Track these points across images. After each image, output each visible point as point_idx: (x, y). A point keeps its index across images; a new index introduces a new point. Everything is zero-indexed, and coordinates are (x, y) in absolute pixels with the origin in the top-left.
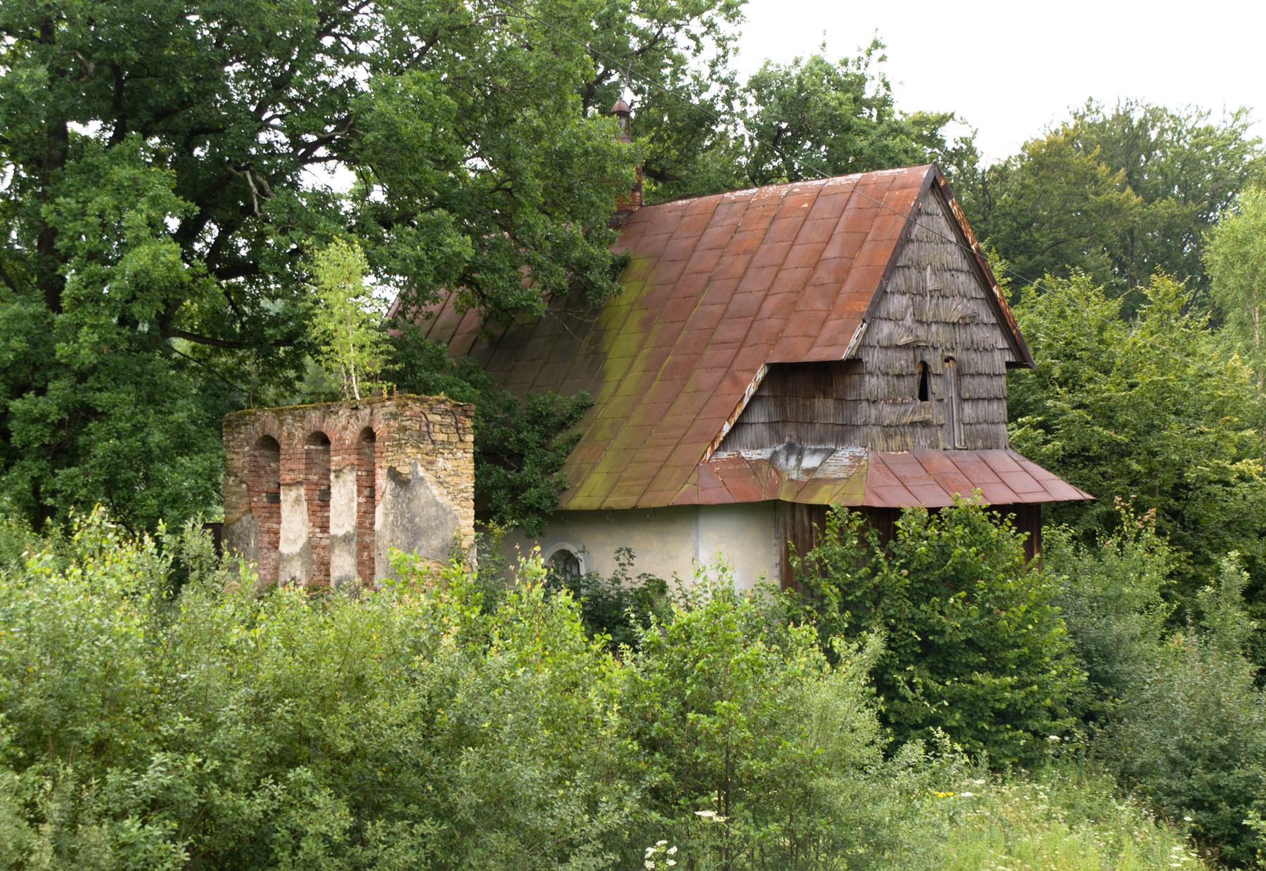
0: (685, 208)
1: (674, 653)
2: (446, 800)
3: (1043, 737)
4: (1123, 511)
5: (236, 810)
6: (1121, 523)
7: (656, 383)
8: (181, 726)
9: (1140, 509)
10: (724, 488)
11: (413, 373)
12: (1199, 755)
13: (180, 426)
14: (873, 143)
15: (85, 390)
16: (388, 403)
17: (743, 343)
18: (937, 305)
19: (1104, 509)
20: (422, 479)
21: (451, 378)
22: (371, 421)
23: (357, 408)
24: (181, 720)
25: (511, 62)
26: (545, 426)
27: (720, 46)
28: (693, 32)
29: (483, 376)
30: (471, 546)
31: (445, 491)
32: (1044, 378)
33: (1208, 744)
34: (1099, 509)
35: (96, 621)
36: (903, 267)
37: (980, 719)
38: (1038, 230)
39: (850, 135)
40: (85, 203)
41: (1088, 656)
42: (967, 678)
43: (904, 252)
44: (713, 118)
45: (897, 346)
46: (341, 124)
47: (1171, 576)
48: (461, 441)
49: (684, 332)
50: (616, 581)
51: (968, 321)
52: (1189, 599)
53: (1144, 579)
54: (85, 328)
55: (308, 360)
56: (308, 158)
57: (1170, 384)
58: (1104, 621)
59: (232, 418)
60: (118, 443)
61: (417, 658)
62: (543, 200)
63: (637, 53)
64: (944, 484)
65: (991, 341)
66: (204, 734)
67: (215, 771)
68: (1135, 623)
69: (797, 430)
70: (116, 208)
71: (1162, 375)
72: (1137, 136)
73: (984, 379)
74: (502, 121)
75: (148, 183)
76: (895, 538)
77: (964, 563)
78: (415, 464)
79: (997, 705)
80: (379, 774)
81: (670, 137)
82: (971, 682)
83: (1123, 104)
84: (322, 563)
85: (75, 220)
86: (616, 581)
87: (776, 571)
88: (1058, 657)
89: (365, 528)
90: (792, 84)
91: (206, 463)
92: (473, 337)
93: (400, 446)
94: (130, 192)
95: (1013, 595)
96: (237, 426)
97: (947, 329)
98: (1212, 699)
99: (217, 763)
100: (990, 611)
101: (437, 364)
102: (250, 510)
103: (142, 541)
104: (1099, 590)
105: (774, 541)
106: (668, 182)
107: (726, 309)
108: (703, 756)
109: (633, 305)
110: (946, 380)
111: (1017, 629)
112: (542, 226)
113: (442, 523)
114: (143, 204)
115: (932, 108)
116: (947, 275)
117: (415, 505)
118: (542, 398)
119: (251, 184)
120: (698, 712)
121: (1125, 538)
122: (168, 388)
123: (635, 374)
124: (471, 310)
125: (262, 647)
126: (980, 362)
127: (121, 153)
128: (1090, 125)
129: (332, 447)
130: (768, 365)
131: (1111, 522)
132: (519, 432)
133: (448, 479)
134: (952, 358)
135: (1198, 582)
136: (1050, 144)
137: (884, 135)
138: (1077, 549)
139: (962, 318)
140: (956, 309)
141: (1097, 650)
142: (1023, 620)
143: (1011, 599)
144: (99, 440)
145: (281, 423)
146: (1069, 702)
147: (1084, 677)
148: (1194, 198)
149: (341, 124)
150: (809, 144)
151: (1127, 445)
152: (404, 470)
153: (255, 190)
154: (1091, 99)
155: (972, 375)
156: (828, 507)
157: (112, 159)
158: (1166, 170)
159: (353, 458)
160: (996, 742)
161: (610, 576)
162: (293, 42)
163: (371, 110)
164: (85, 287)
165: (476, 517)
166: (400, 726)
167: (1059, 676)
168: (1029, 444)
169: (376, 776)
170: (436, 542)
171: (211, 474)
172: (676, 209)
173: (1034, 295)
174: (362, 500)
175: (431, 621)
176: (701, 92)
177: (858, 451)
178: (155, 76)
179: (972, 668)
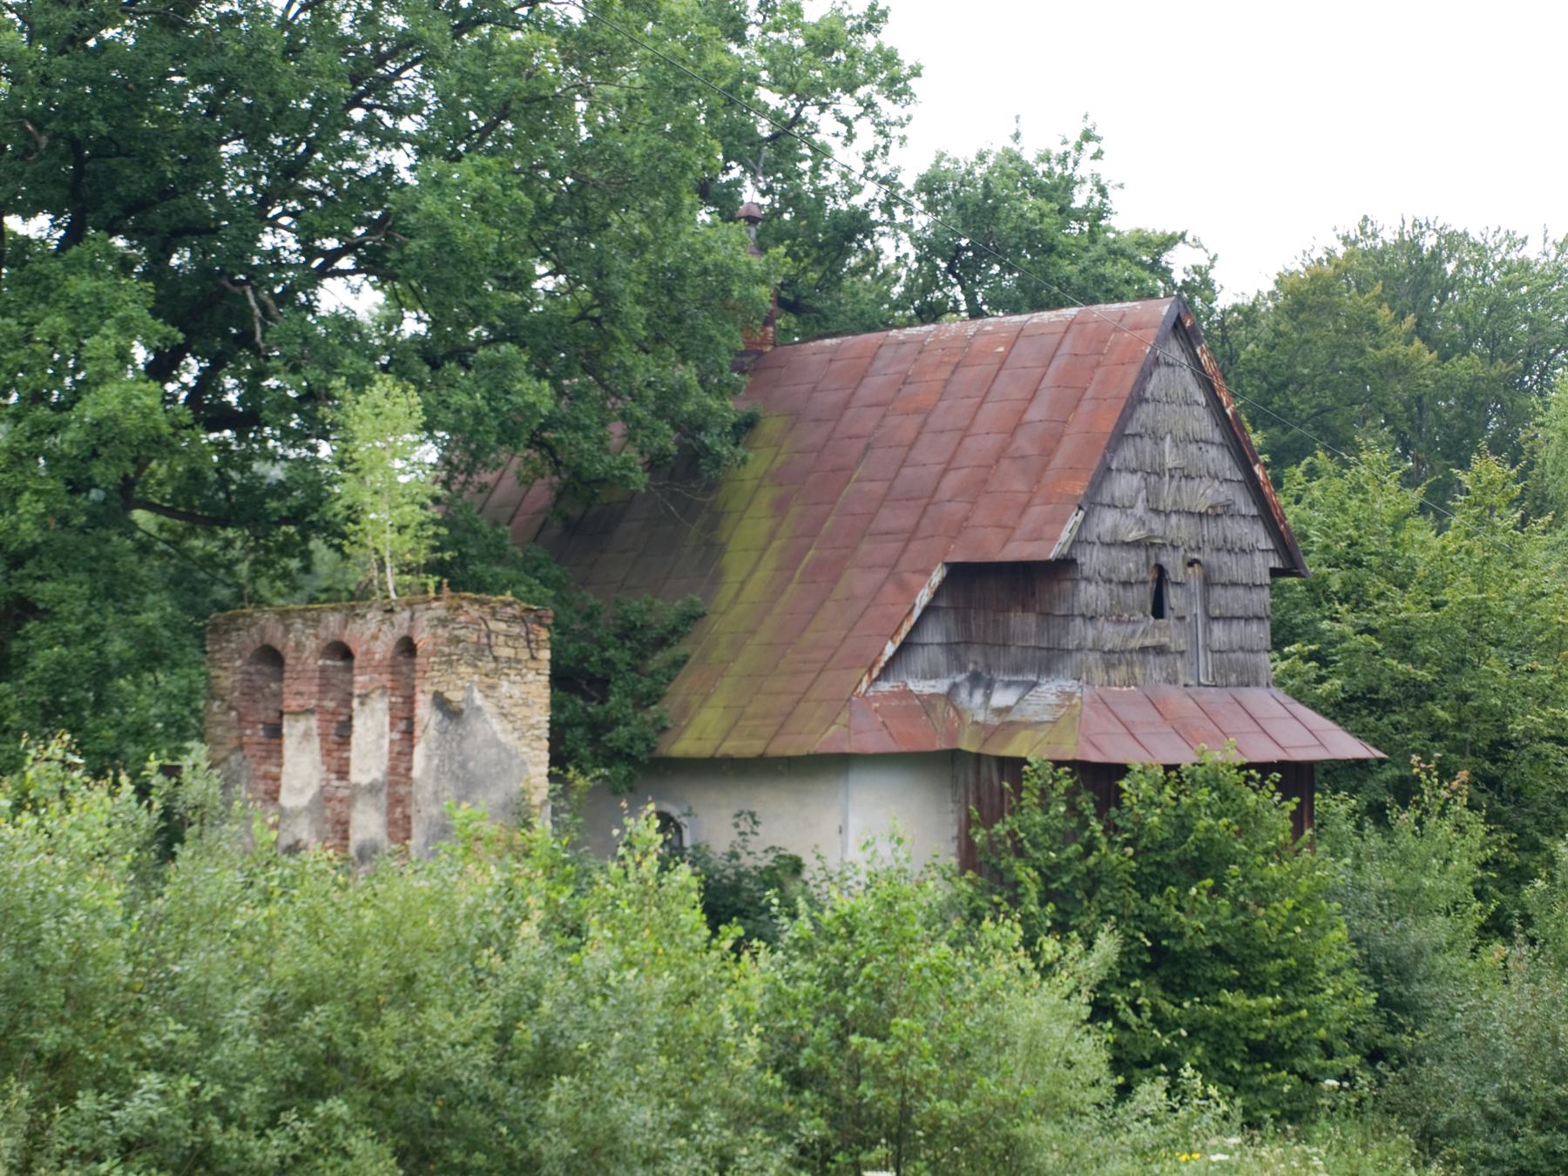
0: (835, 349)
1: (829, 953)
2: (524, 1147)
3: (1314, 1082)
4: (1423, 776)
5: (243, 1154)
6: (1421, 792)
7: (792, 586)
8: (171, 1036)
9: (1446, 773)
10: (885, 732)
11: (464, 566)
12: (1529, 1110)
13: (149, 631)
14: (1084, 270)
15: (22, 579)
16: (434, 604)
17: (912, 534)
18: (1179, 488)
19: (1397, 772)
20: (479, 709)
21: (513, 573)
22: (411, 628)
23: (391, 611)
24: (172, 1028)
25: (608, 146)
26: (639, 642)
27: (881, 133)
28: (844, 114)
29: (555, 571)
30: (544, 803)
31: (510, 727)
32: (1318, 594)
33: (1542, 1094)
34: (1390, 773)
35: (60, 889)
36: (1134, 436)
37: (1229, 1055)
38: (1295, 393)
39: (1054, 258)
40: (31, 325)
41: (1375, 972)
42: (1212, 998)
43: (1136, 415)
44: (868, 228)
45: (1128, 544)
46: (374, 227)
47: (1484, 866)
48: (533, 658)
49: (832, 518)
50: (734, 855)
51: (1219, 511)
52: (1511, 897)
53: (1451, 868)
54: (27, 496)
55: (316, 544)
56: (327, 271)
57: (1491, 603)
58: (1398, 925)
59: (220, 620)
60: (64, 651)
61: (486, 952)
62: (644, 333)
63: (768, 139)
64: (1184, 732)
65: (1251, 539)
66: (201, 1049)
67: (215, 1100)
68: (1439, 927)
69: (986, 656)
70: (72, 332)
71: (1480, 591)
72: (1428, 271)
73: (1240, 591)
74: (591, 226)
75: (115, 299)
76: (1118, 804)
77: (1211, 841)
78: (470, 690)
79: (1253, 1036)
80: (435, 1110)
81: (807, 255)
82: (1218, 1004)
83: (1408, 227)
84: (338, 822)
85: (17, 348)
86: (734, 855)
87: (953, 847)
88: (1336, 972)
89: (399, 774)
90: (975, 187)
91: (184, 682)
92: (540, 520)
93: (450, 663)
94: (97, 311)
95: (1276, 885)
96: (227, 632)
97: (1192, 521)
98: (1547, 1034)
99: (219, 1089)
100: (1244, 908)
101: (497, 554)
102: (241, 747)
103: (116, 783)
104: (1390, 881)
105: (951, 806)
106: (805, 316)
107: (890, 487)
108: (871, 1093)
109: (762, 479)
110: (1189, 590)
111: (1280, 932)
112: (644, 368)
113: (504, 770)
114: (109, 328)
115: (1158, 224)
116: (1193, 448)
117: (468, 745)
118: (636, 604)
119: (253, 303)
120: (862, 1035)
121: (1426, 811)
122: (132, 579)
123: (762, 574)
124: (539, 481)
125: (277, 933)
126: (1235, 568)
127: (79, 259)
128: (1364, 254)
129: (356, 663)
130: (947, 564)
131: (1405, 791)
132: (604, 649)
133: (514, 710)
134: (1197, 561)
135: (1522, 876)
136: (1314, 278)
137: (1099, 260)
138: (1359, 827)
139: (1212, 507)
140: (1204, 494)
141: (1388, 965)
142: (1289, 920)
143: (1274, 891)
144: (40, 646)
145: (287, 629)
146: (1350, 1035)
147: (1371, 1000)
148: (1504, 355)
149: (374, 227)
150: (996, 269)
151: (1428, 685)
152: (455, 696)
153: (257, 312)
154: (1365, 219)
155: (1224, 585)
156: (1024, 761)
157: (67, 265)
158: (1467, 317)
159: (385, 679)
160: (1250, 1088)
161: (727, 849)
162: (313, 115)
163: (415, 209)
164: (29, 439)
165: (552, 762)
166: (465, 1045)
167: (1337, 997)
168: (1296, 682)
169: (430, 1113)
170: (497, 796)
171: (188, 697)
172: (822, 351)
173: (1303, 480)
174: (396, 736)
175: (505, 903)
176: (851, 195)
177: (1069, 685)
178: (127, 155)
179: (1217, 984)
